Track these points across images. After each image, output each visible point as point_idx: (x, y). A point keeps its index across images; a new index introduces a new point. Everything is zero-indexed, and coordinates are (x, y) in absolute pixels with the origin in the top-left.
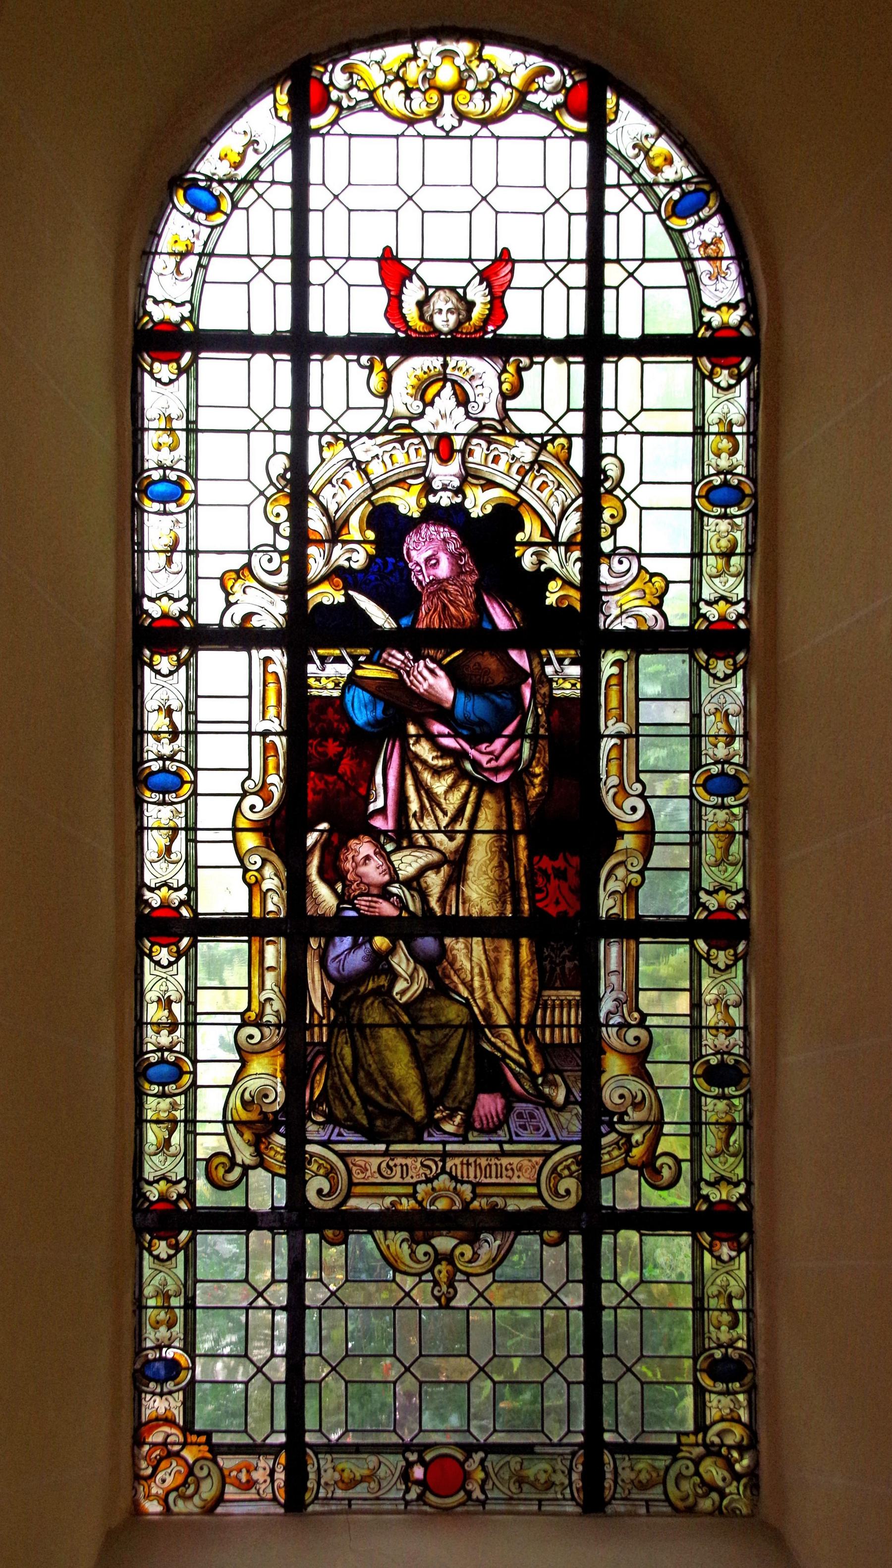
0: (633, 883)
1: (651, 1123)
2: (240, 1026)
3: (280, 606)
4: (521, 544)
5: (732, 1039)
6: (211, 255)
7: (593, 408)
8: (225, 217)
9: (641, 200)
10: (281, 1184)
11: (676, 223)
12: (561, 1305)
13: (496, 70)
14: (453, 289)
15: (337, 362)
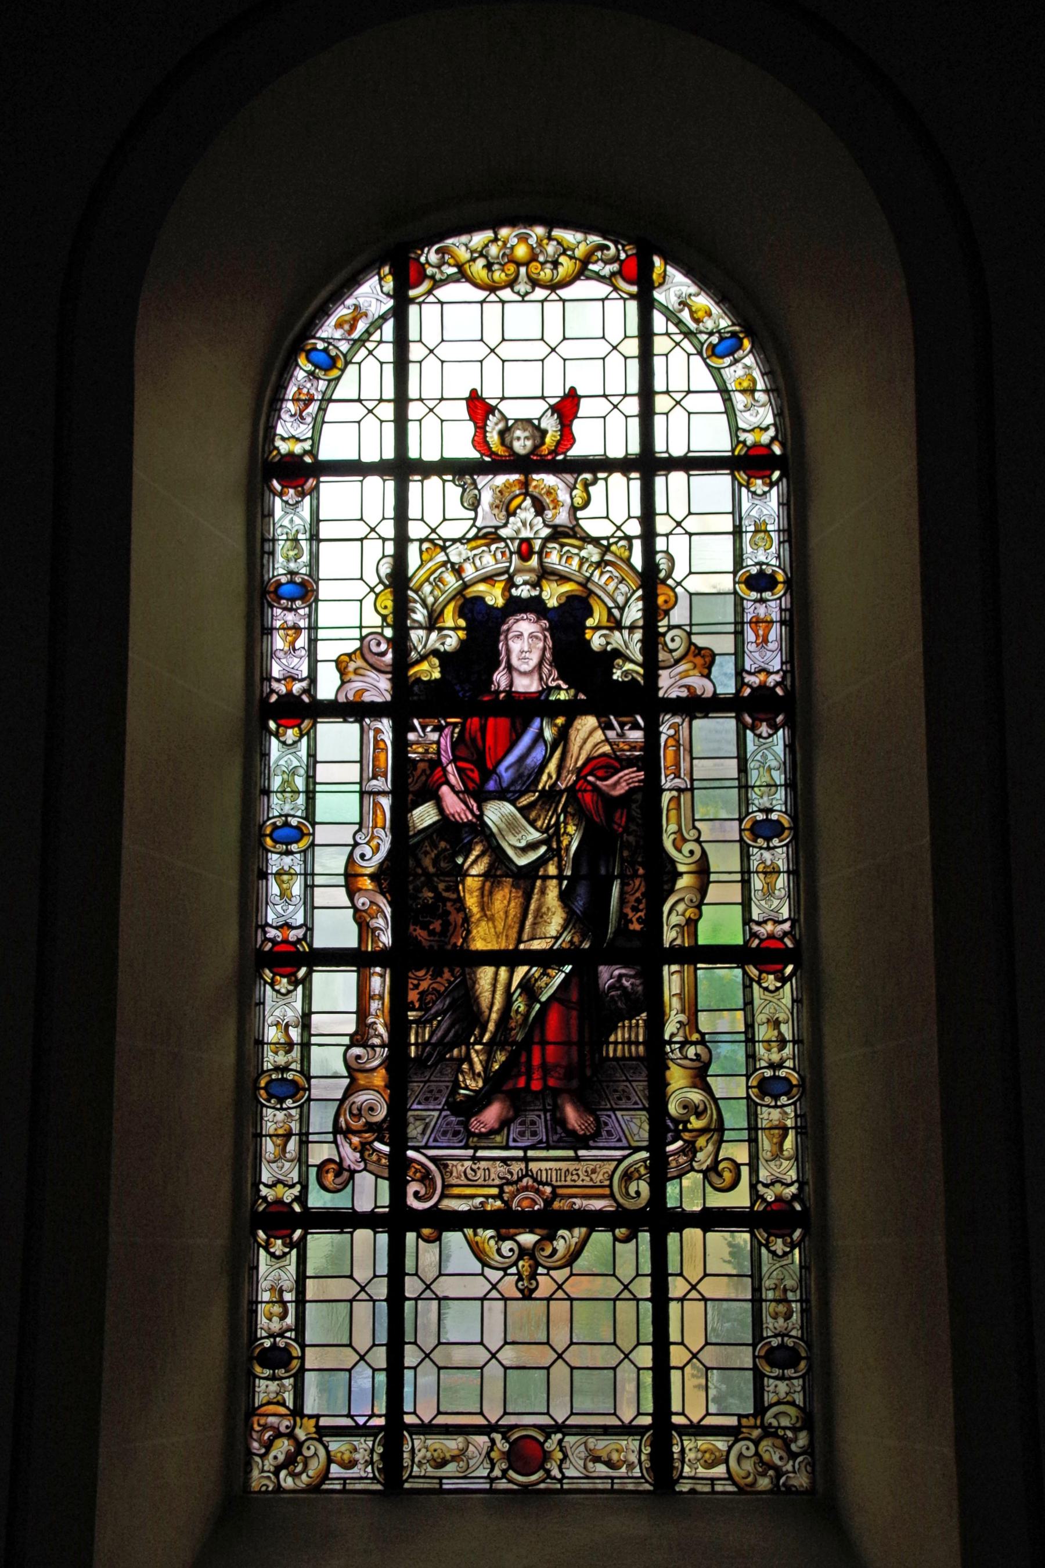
0: (692, 916)
1: (714, 1130)
3: (384, 683)
5: (289, 1057)
6: (330, 400)
9: (686, 344)
10: (384, 1185)
11: (715, 362)
12: (368, 1298)
13: (562, 246)
14: (529, 421)
15: (434, 482)
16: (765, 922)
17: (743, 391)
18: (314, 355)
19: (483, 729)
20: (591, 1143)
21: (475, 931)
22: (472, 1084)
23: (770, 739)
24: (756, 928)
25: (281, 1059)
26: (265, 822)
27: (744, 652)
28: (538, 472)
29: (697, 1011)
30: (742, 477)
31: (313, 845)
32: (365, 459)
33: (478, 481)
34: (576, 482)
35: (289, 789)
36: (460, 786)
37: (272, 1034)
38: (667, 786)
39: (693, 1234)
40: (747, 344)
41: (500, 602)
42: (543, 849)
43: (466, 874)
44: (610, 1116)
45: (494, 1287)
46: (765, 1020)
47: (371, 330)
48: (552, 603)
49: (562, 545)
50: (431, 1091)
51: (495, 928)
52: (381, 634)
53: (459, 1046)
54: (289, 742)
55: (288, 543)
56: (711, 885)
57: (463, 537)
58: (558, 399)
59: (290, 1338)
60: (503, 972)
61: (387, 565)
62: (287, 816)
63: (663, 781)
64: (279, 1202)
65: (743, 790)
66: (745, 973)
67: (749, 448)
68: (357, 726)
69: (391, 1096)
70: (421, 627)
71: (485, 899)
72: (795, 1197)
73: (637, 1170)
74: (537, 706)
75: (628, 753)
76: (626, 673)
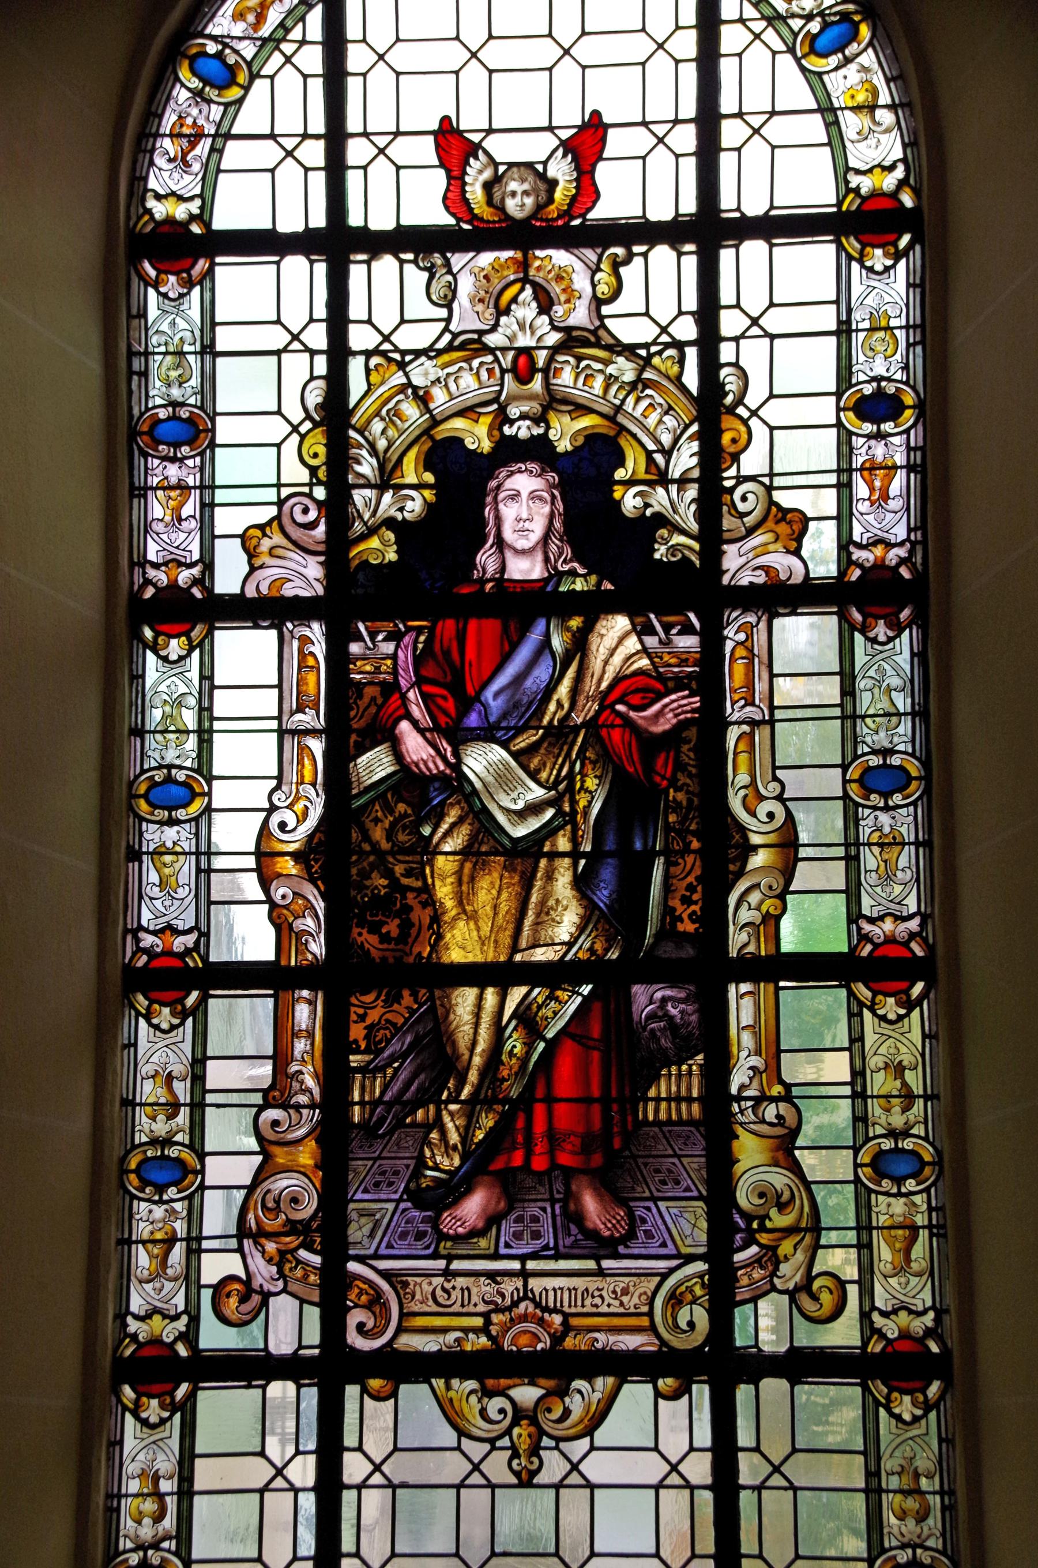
0: (772, 911)
1: (806, 1230)
2: (261, 1109)
3: (314, 569)
4: (621, 483)
5: (173, 1123)
6: (229, 136)
7: (708, 312)
8: (242, 92)
9: (770, 36)
10: (313, 1314)
11: (814, 63)
14: (530, 165)
15: (386, 265)
16: (881, 918)
17: (856, 109)
18: (201, 63)
19: (461, 637)
20: (621, 1249)
21: (448, 936)
22: (445, 1162)
23: (891, 645)
24: (867, 927)
25: (161, 1127)
26: (137, 777)
27: (851, 514)
28: (543, 247)
29: (779, 1051)
30: (852, 245)
31: (209, 810)
32: (283, 228)
33: (453, 261)
34: (600, 260)
35: (173, 728)
36: (427, 722)
37: (149, 1091)
39: (774, 1387)
40: (865, 31)
41: (486, 446)
42: (550, 813)
43: (436, 852)
44: (649, 1209)
45: (476, 1467)
46: (881, 1065)
47: (289, 23)
48: (564, 446)
49: (579, 359)
50: (383, 1173)
51: (478, 929)
52: (310, 496)
53: (424, 1104)
54: (173, 657)
55: (169, 358)
56: (800, 864)
57: (431, 348)
58: (575, 131)
59: (169, 1551)
60: (491, 996)
61: (316, 392)
62: (170, 767)
63: (729, 710)
64: (156, 1341)
65: (848, 723)
66: (851, 994)
67: (864, 199)
68: (273, 633)
69: (323, 1181)
71: (464, 888)
72: (929, 1332)
73: (690, 1290)
74: (538, 601)
75: (676, 670)
76: (673, 549)
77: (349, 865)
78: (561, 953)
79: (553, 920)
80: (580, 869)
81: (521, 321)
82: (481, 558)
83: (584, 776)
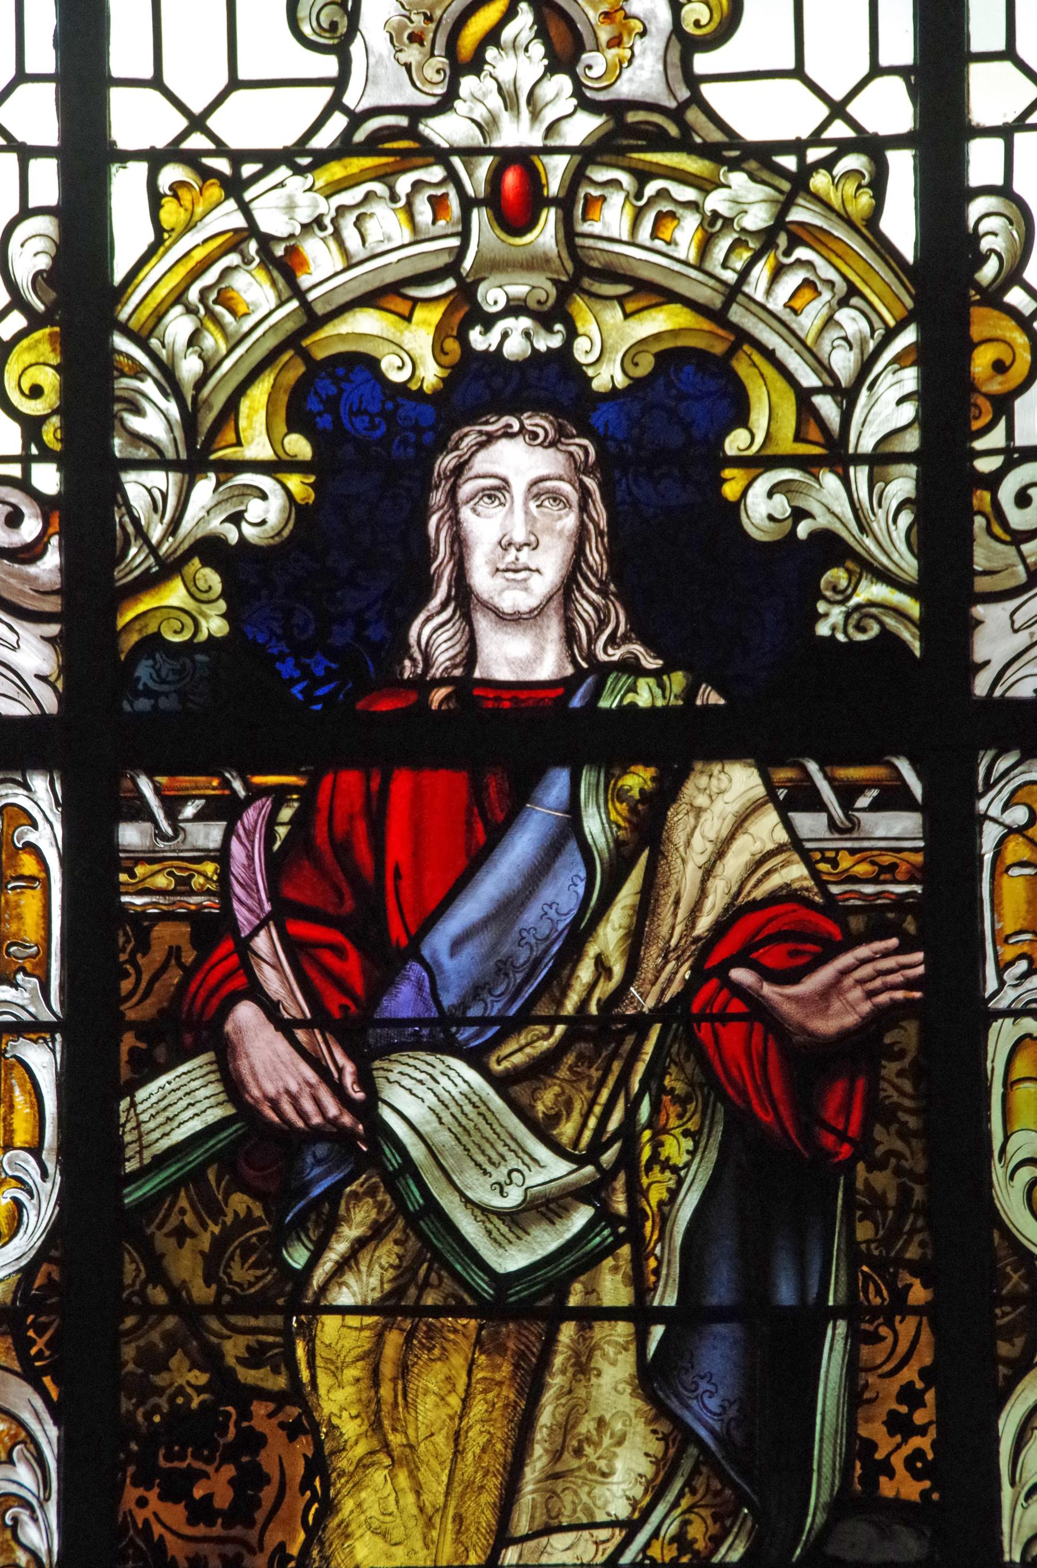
21: (348, 1505)
36: (295, 1005)
38: (1002, 1002)
41: (431, 375)
42: (581, 1216)
48: (608, 375)
49: (643, 176)
52: (24, 484)
57: (301, 146)
61: (40, 244)
63: (992, 984)
70: (161, 463)
71: (386, 1391)
75: (869, 889)
77: (116, 1338)
78: (611, 1547)
79: (592, 1468)
80: (652, 1347)
81: (508, 86)
82: (419, 630)
83: (659, 1131)
